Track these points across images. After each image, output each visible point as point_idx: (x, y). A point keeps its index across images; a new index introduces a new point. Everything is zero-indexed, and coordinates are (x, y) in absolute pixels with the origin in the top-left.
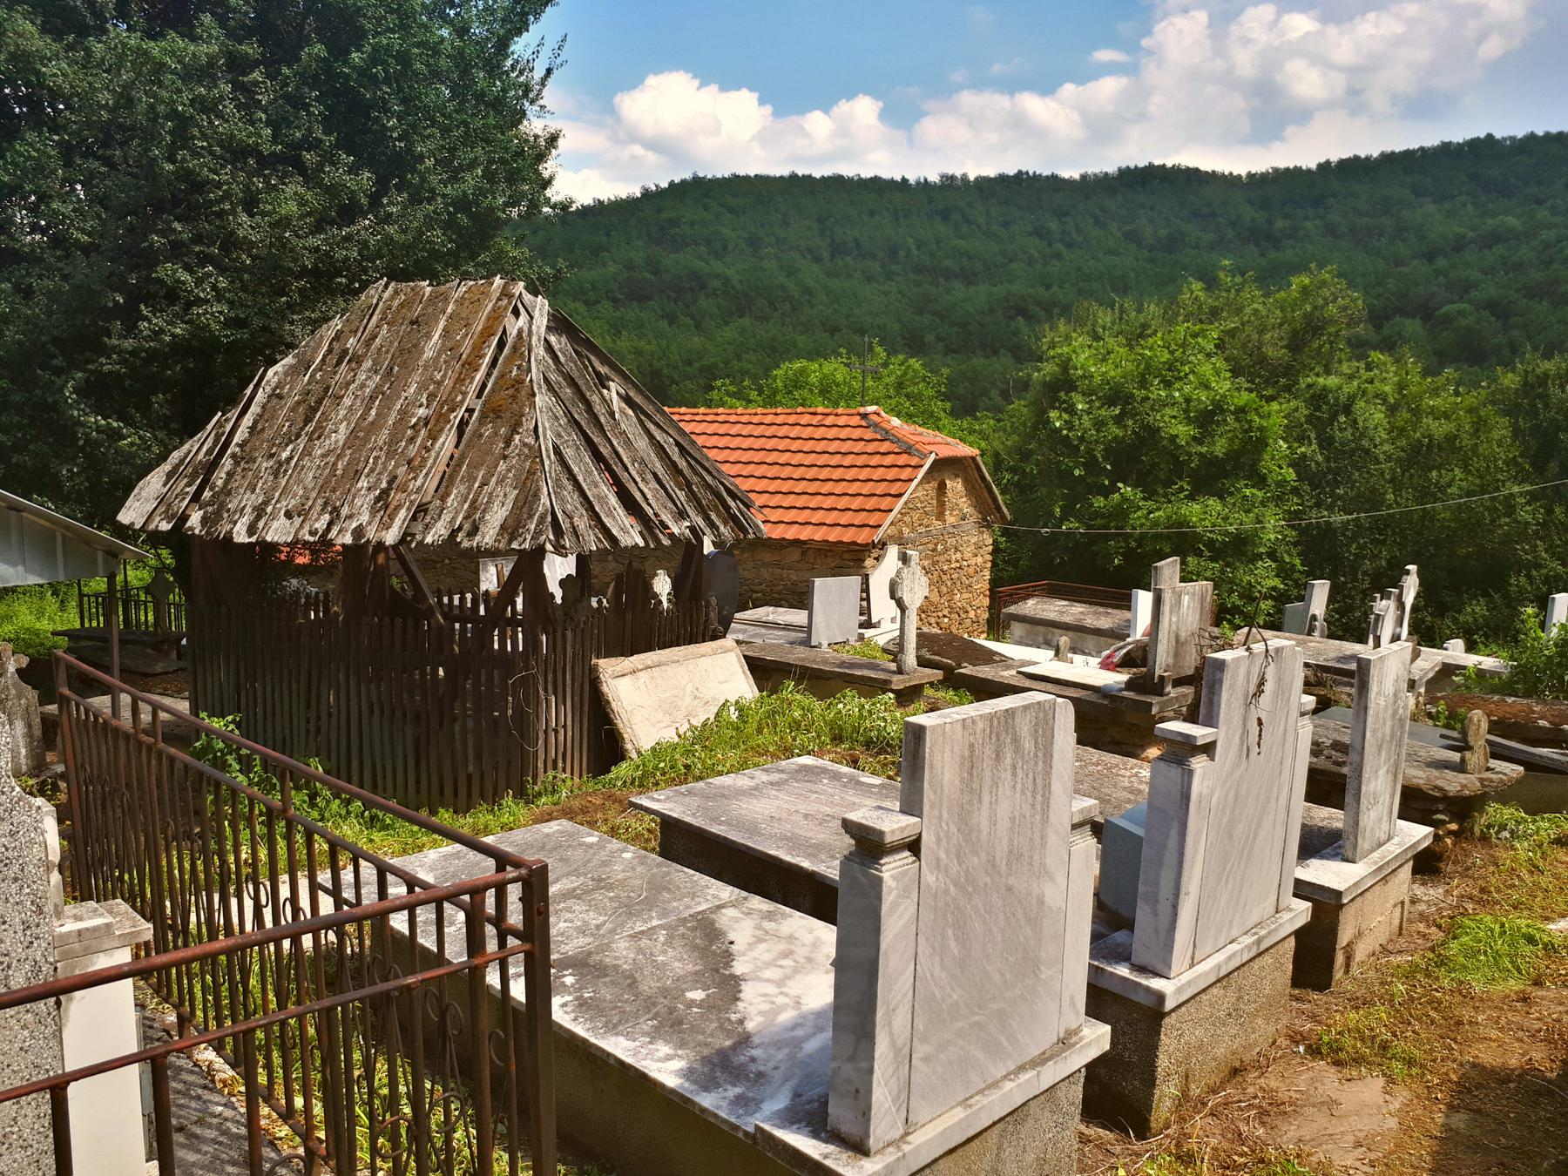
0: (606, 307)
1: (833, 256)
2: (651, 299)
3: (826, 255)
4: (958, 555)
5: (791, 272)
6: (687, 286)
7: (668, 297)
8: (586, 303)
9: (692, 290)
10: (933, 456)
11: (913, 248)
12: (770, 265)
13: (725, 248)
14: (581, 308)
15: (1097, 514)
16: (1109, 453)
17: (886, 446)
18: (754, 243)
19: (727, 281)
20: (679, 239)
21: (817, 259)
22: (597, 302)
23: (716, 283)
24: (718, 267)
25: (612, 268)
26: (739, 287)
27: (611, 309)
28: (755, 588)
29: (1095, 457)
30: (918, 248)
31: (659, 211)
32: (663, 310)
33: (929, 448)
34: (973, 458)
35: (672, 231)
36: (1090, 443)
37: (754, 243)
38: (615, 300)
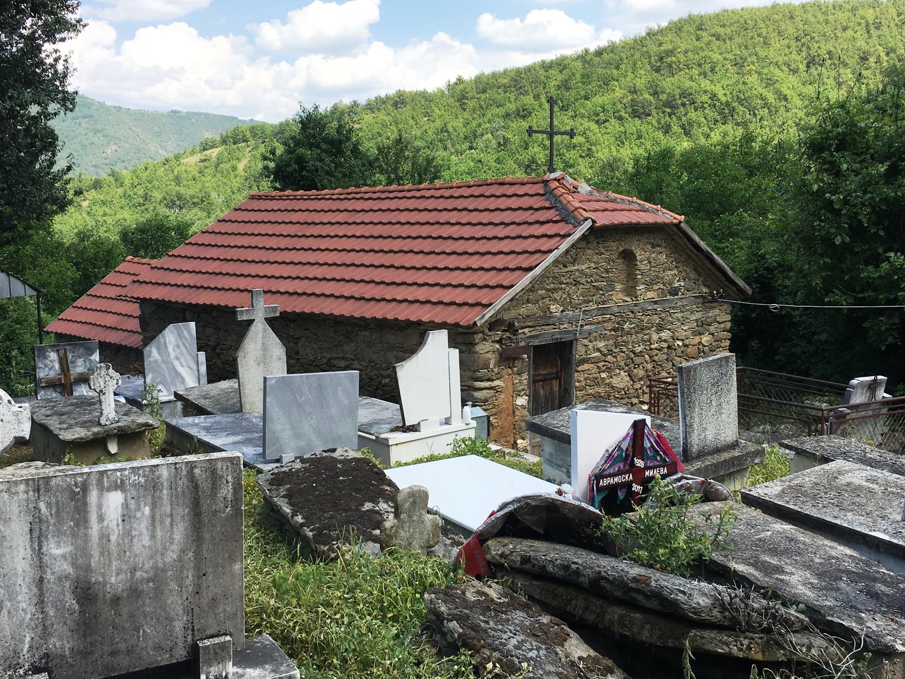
0: (614, 126)
1: (808, 67)
2: (649, 115)
3: (802, 67)
4: (665, 334)
5: (770, 83)
6: (679, 102)
7: (664, 112)
8: (597, 122)
9: (684, 105)
10: (588, 224)
11: (883, 55)
12: (753, 79)
13: (712, 70)
14: (594, 126)
15: (870, 285)
16: (878, 215)
17: (551, 214)
18: (739, 64)
19: (713, 96)
20: (674, 66)
21: (795, 72)
22: (606, 121)
23: (705, 98)
24: (705, 84)
25: (619, 93)
26: (723, 99)
27: (617, 126)
28: (383, 373)
29: (860, 222)
30: (888, 54)
31: (660, 45)
32: (659, 123)
33: (586, 215)
34: (678, 226)
35: (669, 59)
36: (855, 206)
37: (739, 64)
38: (620, 118)
